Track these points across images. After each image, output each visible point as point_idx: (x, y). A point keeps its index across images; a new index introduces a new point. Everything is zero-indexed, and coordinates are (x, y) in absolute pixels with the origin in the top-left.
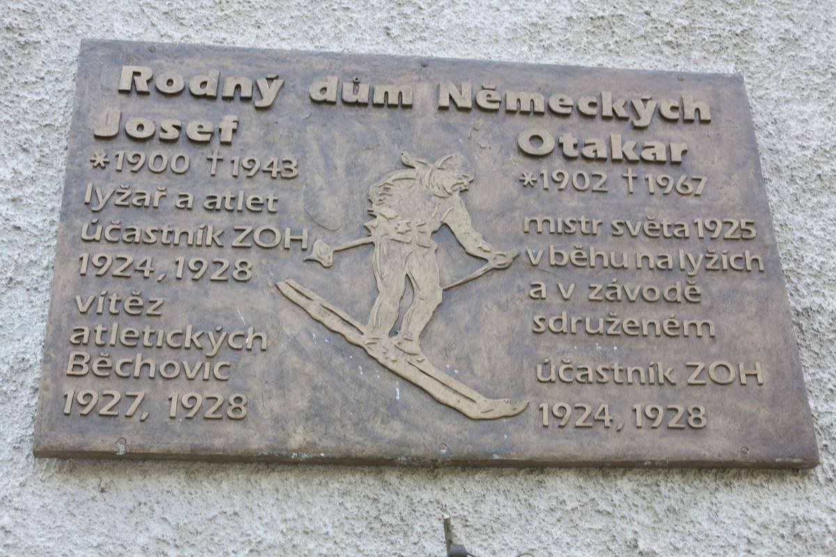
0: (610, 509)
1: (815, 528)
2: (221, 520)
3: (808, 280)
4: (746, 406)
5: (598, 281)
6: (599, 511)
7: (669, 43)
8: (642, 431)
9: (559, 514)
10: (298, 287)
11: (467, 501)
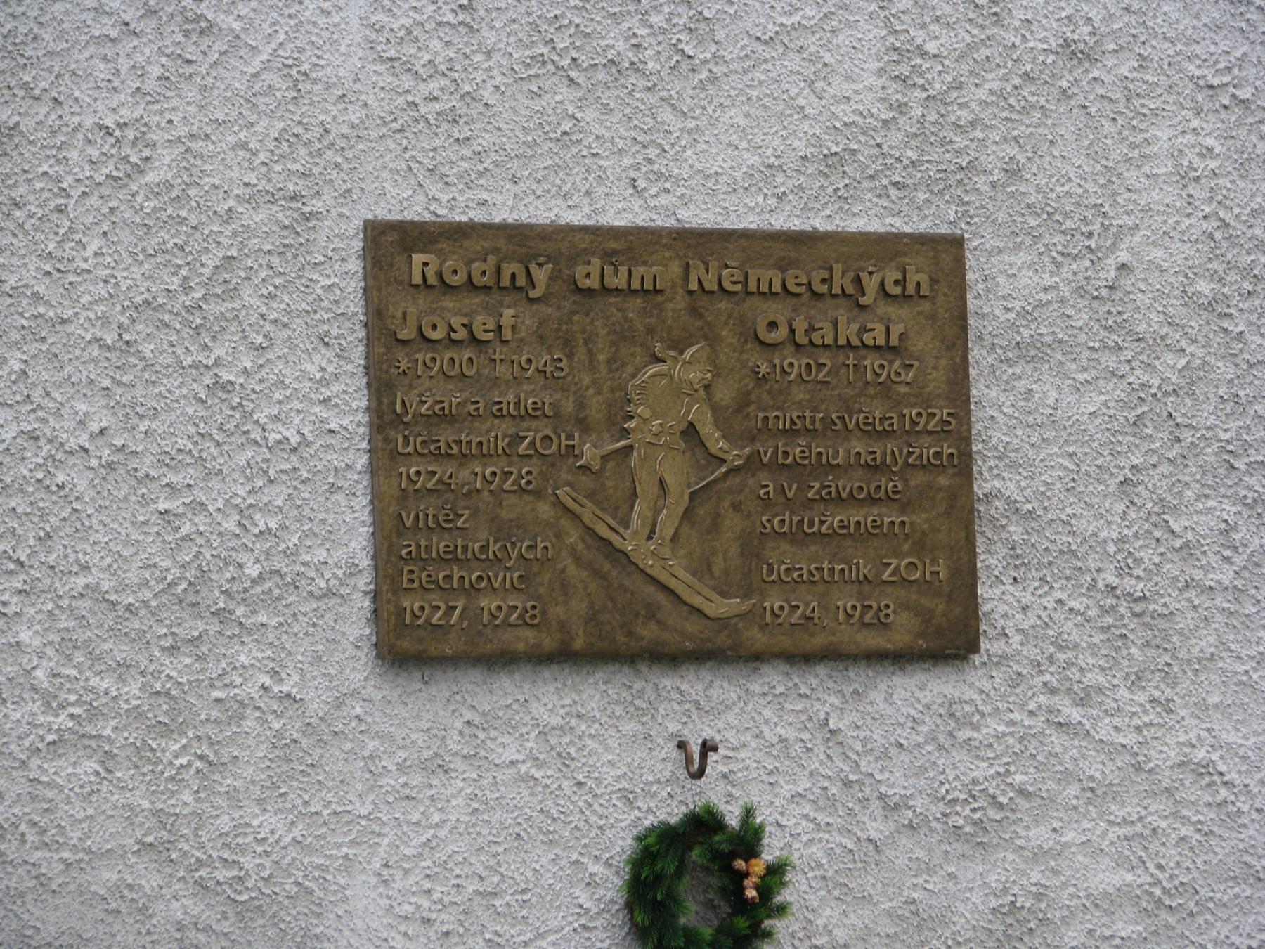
0: (808, 692)
1: (967, 708)
2: (515, 707)
3: (992, 463)
4: (926, 602)
5: (815, 480)
6: (800, 695)
7: (895, 184)
8: (843, 627)
9: (770, 698)
10: (574, 494)
11: (700, 687)
